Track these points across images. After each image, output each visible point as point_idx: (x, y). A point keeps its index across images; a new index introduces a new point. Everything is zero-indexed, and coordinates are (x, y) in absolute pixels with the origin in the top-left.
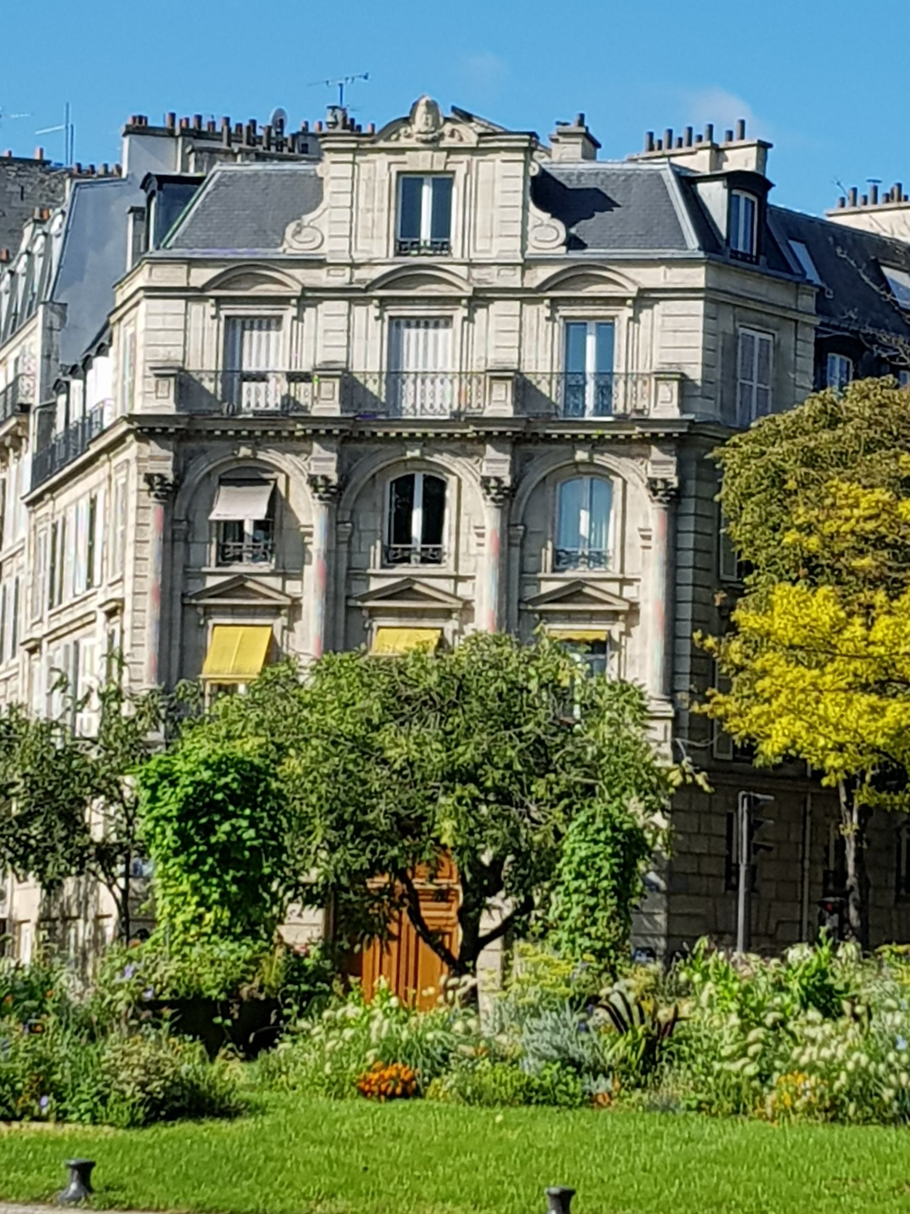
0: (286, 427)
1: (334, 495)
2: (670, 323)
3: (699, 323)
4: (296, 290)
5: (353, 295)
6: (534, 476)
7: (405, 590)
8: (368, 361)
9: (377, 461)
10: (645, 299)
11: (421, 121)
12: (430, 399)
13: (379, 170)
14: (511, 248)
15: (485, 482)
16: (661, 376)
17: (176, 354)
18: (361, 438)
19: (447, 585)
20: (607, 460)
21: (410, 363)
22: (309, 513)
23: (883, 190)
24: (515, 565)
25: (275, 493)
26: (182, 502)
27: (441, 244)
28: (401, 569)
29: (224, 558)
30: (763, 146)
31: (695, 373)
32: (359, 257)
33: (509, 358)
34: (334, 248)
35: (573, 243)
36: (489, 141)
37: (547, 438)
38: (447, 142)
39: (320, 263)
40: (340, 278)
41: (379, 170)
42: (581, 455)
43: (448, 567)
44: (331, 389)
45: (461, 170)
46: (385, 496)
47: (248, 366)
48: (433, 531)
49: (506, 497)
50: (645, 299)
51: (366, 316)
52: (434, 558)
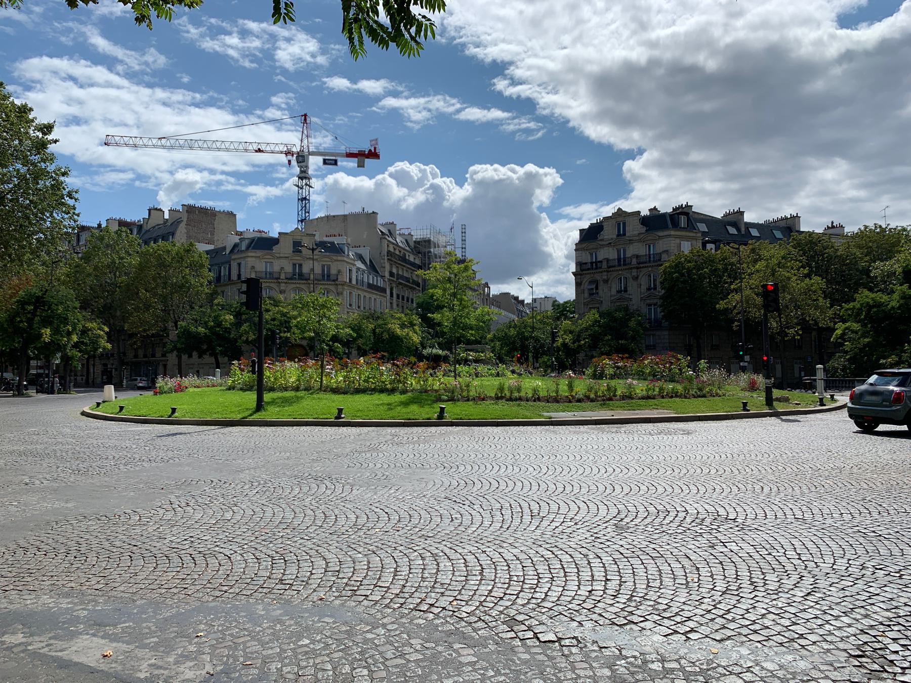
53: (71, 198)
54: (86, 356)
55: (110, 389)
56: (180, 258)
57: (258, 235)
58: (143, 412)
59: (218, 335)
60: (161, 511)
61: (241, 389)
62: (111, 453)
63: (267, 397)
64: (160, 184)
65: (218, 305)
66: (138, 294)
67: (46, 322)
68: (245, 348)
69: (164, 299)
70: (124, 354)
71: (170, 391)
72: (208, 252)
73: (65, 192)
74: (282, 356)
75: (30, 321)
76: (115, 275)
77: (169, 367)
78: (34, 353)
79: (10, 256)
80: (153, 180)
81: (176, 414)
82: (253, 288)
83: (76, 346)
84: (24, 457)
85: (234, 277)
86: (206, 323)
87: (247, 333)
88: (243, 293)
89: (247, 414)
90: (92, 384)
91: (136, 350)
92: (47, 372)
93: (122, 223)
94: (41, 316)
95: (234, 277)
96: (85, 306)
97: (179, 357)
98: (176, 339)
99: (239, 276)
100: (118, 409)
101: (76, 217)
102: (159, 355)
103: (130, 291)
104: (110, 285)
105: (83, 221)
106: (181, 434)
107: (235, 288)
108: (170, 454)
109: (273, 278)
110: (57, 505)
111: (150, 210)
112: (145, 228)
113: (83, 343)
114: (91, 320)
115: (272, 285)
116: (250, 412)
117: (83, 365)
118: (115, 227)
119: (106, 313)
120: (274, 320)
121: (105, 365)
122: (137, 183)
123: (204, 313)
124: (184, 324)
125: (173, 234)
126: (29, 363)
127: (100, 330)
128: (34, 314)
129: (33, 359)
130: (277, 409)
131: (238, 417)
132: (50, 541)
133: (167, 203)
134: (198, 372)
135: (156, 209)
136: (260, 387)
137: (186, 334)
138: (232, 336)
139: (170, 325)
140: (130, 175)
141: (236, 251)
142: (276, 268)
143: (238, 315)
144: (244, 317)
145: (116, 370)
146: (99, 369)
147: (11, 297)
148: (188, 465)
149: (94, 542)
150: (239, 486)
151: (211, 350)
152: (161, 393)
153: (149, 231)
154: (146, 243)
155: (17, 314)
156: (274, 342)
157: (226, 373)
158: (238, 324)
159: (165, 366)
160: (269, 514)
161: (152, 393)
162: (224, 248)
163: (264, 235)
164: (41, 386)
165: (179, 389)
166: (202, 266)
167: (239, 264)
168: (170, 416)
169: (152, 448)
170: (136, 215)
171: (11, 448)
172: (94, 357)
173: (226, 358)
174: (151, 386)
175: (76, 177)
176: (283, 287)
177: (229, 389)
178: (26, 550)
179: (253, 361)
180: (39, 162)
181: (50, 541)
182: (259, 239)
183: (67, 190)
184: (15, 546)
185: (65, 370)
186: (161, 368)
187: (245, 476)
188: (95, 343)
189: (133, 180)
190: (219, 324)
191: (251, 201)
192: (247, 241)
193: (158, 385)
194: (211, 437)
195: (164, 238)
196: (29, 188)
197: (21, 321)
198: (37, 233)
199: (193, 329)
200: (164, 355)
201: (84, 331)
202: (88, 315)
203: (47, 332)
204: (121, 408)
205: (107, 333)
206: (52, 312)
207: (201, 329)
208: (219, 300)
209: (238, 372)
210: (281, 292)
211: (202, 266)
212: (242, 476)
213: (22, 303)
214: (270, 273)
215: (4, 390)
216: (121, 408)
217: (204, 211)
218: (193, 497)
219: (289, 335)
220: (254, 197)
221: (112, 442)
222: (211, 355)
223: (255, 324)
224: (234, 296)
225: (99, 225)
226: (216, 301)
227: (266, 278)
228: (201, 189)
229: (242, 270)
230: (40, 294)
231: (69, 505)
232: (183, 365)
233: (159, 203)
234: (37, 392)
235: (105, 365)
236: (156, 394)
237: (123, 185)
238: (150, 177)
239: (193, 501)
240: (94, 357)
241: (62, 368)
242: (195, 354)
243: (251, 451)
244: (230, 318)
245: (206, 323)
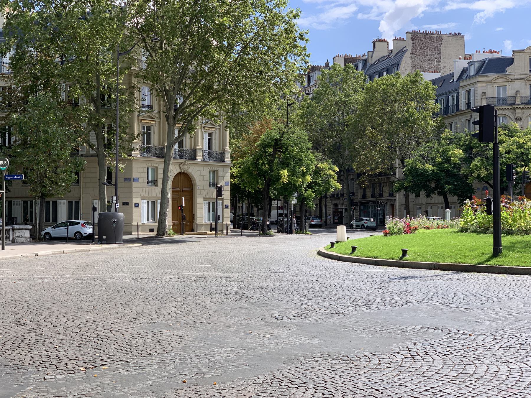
53: (302, 40)
54: (319, 196)
55: (342, 229)
56: (406, 89)
57: (490, 56)
58: (374, 254)
59: (447, 172)
60: (400, 358)
61: (475, 231)
62: (347, 293)
63: (505, 240)
64: (382, 14)
65: (446, 139)
66: (364, 131)
67: (284, 164)
68: (476, 185)
69: (390, 136)
70: (353, 194)
71: (399, 232)
72: (434, 82)
73: (297, 35)
74: (520, 194)
75: (271, 163)
76: (343, 113)
77: (396, 207)
78: (274, 194)
79: (253, 102)
80: (375, 10)
81: (407, 257)
82: (487, 116)
83: (310, 186)
84: (272, 293)
85: (463, 106)
86: (433, 159)
87: (478, 168)
88: (475, 123)
89: (482, 259)
90: (327, 225)
91: (364, 190)
92: (286, 212)
93: (348, 60)
94: (279, 158)
95: (463, 106)
96: (315, 148)
97: (407, 197)
98: (403, 177)
99: (468, 105)
100: (351, 250)
101: (306, 58)
102: (386, 194)
103: (358, 129)
104: (338, 123)
105: (312, 62)
106: (413, 277)
107: (464, 119)
108: (404, 298)
109: (507, 105)
110: (304, 341)
111: (374, 43)
112: (370, 62)
113: (316, 183)
114: (322, 160)
115: (506, 112)
116: (487, 257)
117: (316, 205)
118: (341, 63)
119: (335, 153)
120: (508, 152)
121: (336, 205)
122: (360, 16)
123: (432, 148)
124: (410, 161)
125: (398, 65)
126: (270, 204)
127: (330, 169)
128: (273, 155)
129: (273, 199)
130: (518, 255)
131: (474, 262)
132: (300, 375)
133: (389, 31)
134: (426, 212)
135: (380, 41)
136: (497, 231)
137: (414, 172)
138: (462, 172)
139: (397, 163)
140: (353, 9)
141: (464, 77)
142: (511, 93)
143: (468, 148)
144: (474, 151)
145: (346, 210)
146: (331, 209)
147: (255, 141)
148: (423, 311)
149: (339, 381)
150: (480, 339)
151: (443, 188)
152: (391, 234)
153: (374, 64)
154: (371, 78)
155: (260, 157)
156: (510, 178)
157: (458, 214)
158: (468, 159)
159: (393, 206)
160: (516, 372)
161: (382, 234)
162: (452, 75)
163: (496, 56)
164: (282, 226)
165: (409, 230)
166: (428, 97)
167: (469, 92)
168: (401, 259)
169: (386, 291)
170: (360, 50)
171: (262, 284)
172: (326, 197)
173: (456, 198)
174: (380, 226)
175: (303, 18)
176: (518, 113)
177: (462, 231)
178: (281, 381)
179: (488, 200)
180: (274, 8)
181: (300, 375)
182: (491, 60)
183: (299, 32)
184: (271, 377)
185: (301, 210)
186: (388, 209)
187: (486, 328)
188: (326, 182)
189: (356, 13)
190: (447, 160)
191: (478, 18)
192: (477, 65)
193: (387, 226)
194: (445, 282)
195: (389, 71)
196: (266, 35)
197: (263, 164)
198: (272, 78)
199: (420, 166)
200: (391, 195)
201: (317, 172)
202: (319, 155)
203: (285, 173)
204: (354, 249)
205: (337, 173)
206: (289, 154)
207: (429, 167)
208: (447, 133)
209: (471, 212)
210: (517, 120)
211: (428, 97)
212: (482, 327)
213: (264, 146)
214: (504, 99)
215: (251, 229)
216: (354, 249)
217: (429, 36)
218: (432, 345)
219: (526, 169)
220: (482, 14)
221: (347, 283)
222: (440, 193)
223: (487, 159)
224: (465, 128)
225: (327, 64)
226: (443, 135)
227: (499, 105)
228: (423, 12)
229: (472, 98)
230: (278, 137)
231: (314, 342)
232: (411, 204)
233: (381, 34)
234: (278, 232)
235: (336, 205)
236: (386, 235)
237: (346, 19)
238: (372, 8)
239: (432, 350)
240: (326, 197)
241: (298, 210)
242: (423, 193)
243: (490, 300)
244: (459, 152)
245: (433, 159)
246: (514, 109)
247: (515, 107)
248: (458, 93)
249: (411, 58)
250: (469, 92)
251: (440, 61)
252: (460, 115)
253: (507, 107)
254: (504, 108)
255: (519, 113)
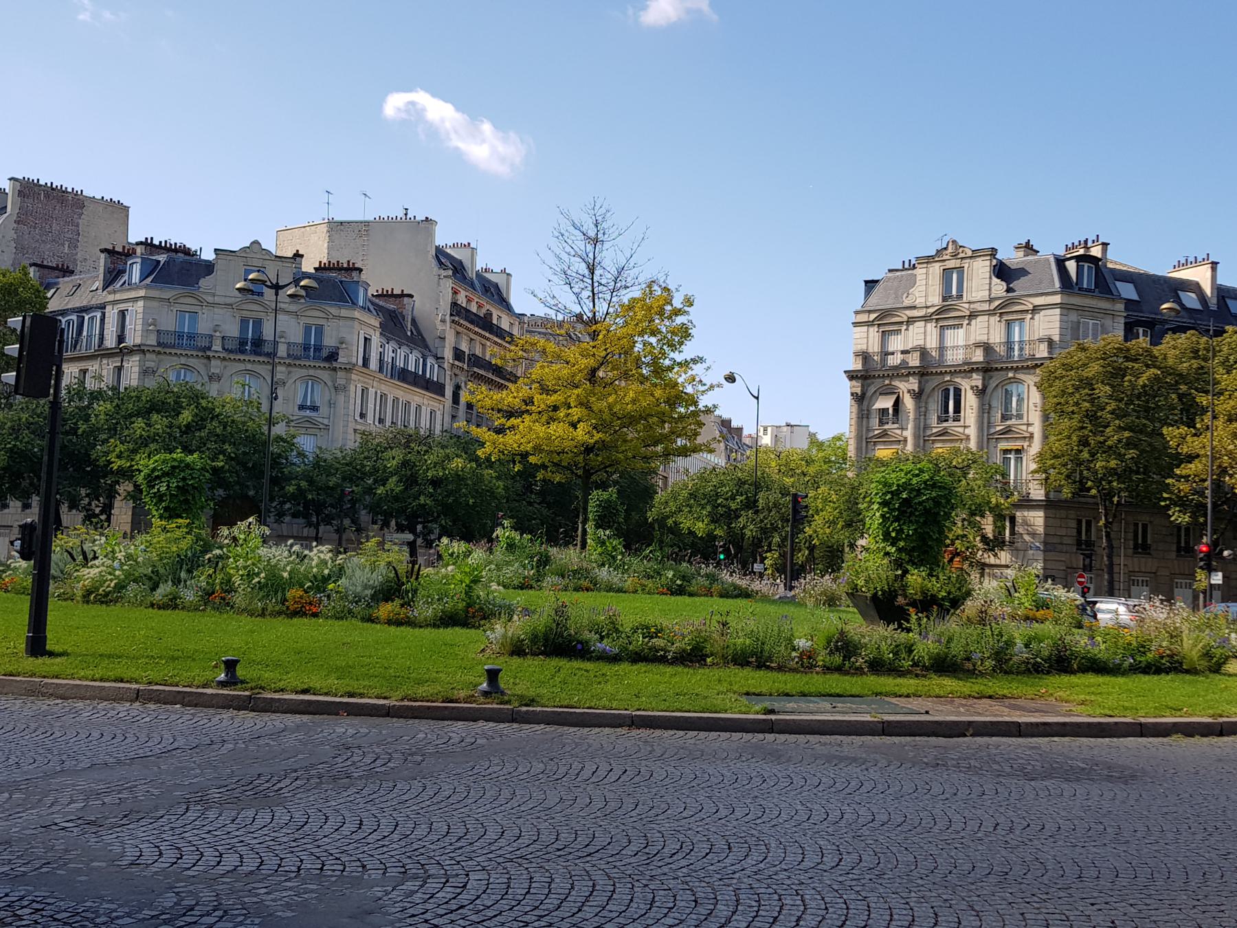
0: (902, 372)
1: (918, 396)
2: (1047, 319)
3: (1058, 318)
4: (905, 319)
5: (926, 319)
6: (993, 384)
7: (944, 433)
8: (932, 343)
9: (933, 382)
10: (1036, 309)
11: (950, 250)
12: (955, 357)
13: (936, 269)
14: (984, 295)
15: (972, 388)
16: (1041, 340)
17: (864, 347)
18: (927, 374)
19: (961, 430)
20: (1020, 376)
21: (949, 342)
22: (909, 403)
23: (1199, 259)
24: (986, 421)
25: (898, 398)
26: (865, 403)
27: (960, 297)
28: (945, 424)
29: (881, 423)
30: (1105, 245)
31: (1056, 338)
32: (929, 304)
33: (984, 338)
34: (920, 301)
35: (1009, 290)
36: (976, 254)
37: (997, 369)
38: (961, 255)
39: (914, 307)
40: (922, 313)
41: (936, 269)
42: (1011, 375)
43: (1025, 421)
44: (917, 355)
45: (966, 266)
46: (938, 396)
47: (891, 349)
48: (957, 409)
49: (981, 393)
50: (1036, 309)
51: (931, 326)
52: (957, 419)
85: (110, 342)
167: (123, 314)
214: (191, 337)
236: (993, 252)
246: (208, 358)
247: (211, 354)
248: (104, 315)
249: (16, 230)
250: (123, 314)
251: (76, 247)
252: (103, 356)
253: (195, 353)
254: (189, 353)
255: (216, 367)
